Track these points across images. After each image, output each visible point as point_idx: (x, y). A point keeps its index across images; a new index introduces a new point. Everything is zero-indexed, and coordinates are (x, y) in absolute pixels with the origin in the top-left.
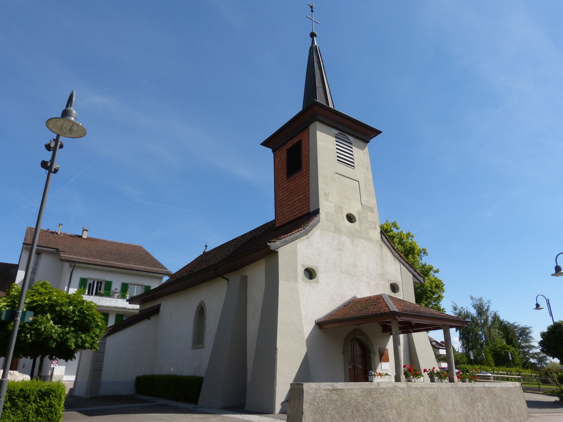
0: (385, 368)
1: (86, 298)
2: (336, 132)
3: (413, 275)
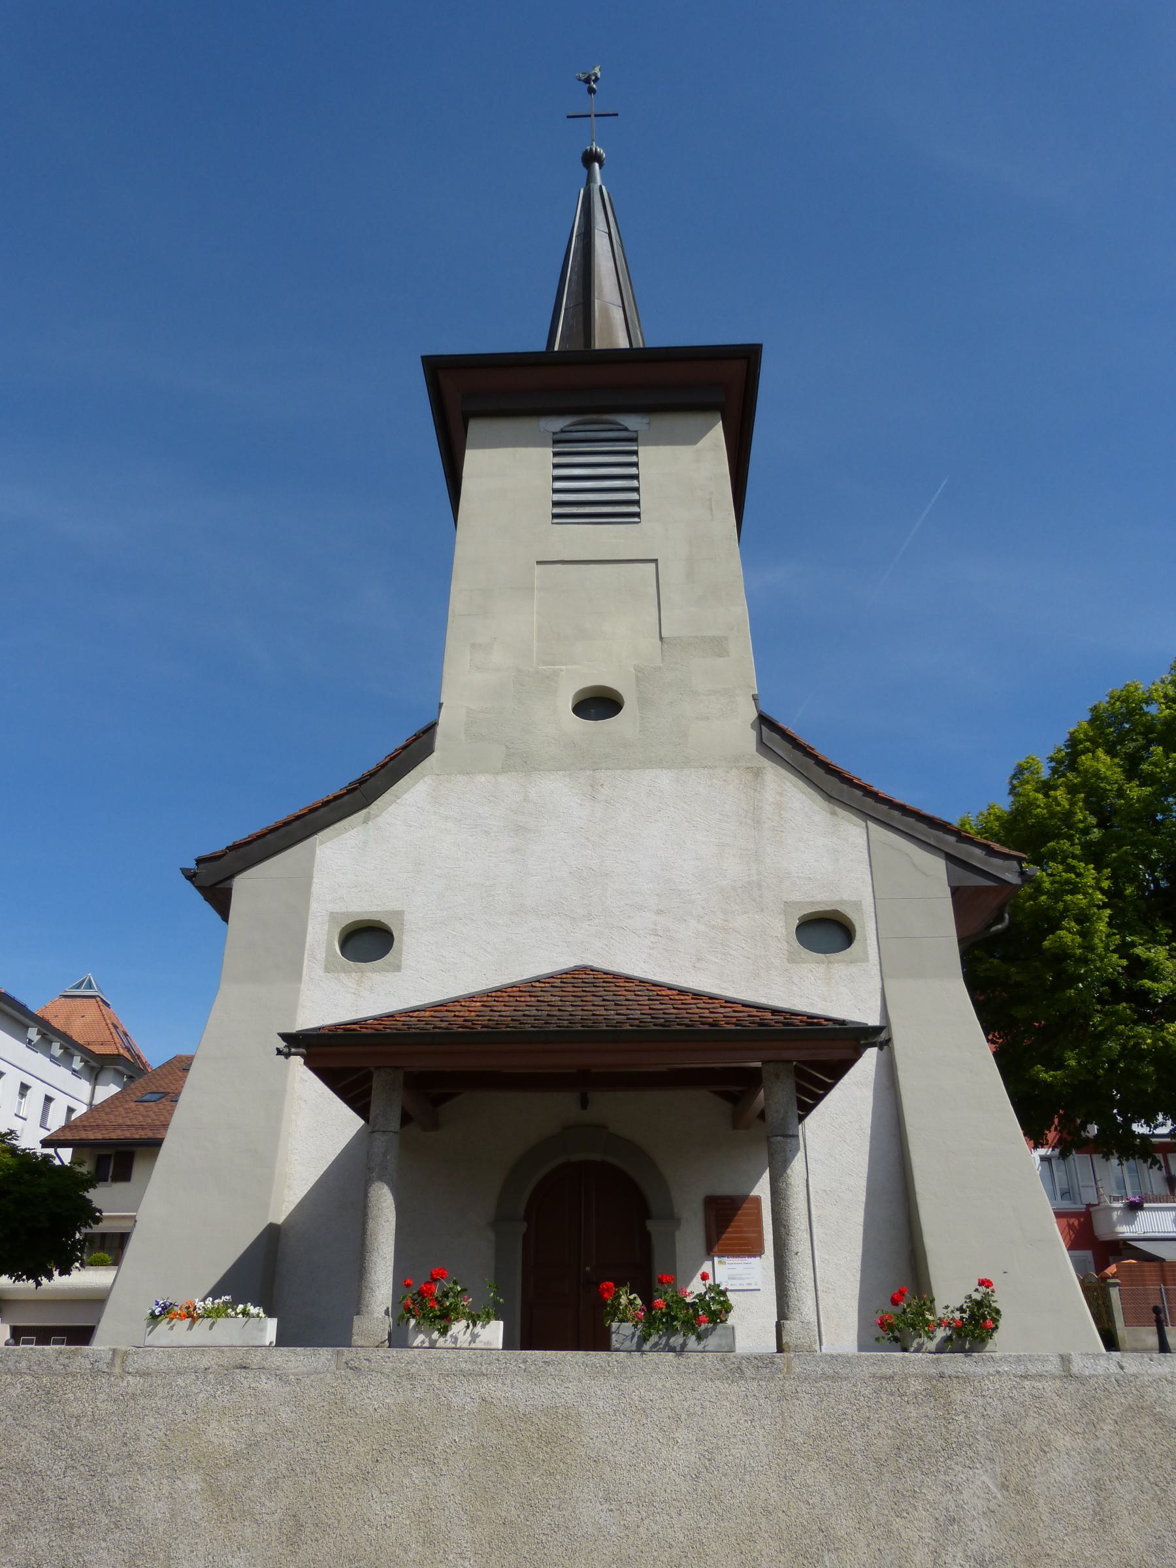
0: (737, 1282)
1: (1054, 1126)
2: (557, 424)
3: (950, 858)
